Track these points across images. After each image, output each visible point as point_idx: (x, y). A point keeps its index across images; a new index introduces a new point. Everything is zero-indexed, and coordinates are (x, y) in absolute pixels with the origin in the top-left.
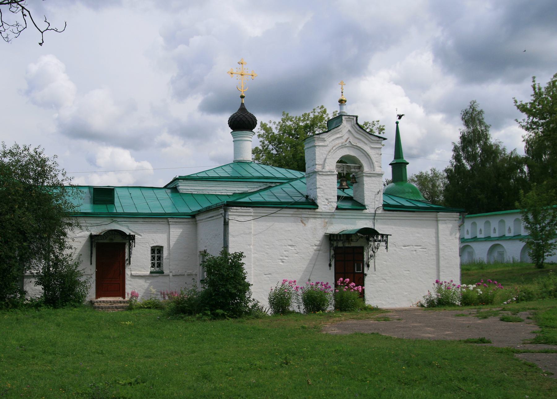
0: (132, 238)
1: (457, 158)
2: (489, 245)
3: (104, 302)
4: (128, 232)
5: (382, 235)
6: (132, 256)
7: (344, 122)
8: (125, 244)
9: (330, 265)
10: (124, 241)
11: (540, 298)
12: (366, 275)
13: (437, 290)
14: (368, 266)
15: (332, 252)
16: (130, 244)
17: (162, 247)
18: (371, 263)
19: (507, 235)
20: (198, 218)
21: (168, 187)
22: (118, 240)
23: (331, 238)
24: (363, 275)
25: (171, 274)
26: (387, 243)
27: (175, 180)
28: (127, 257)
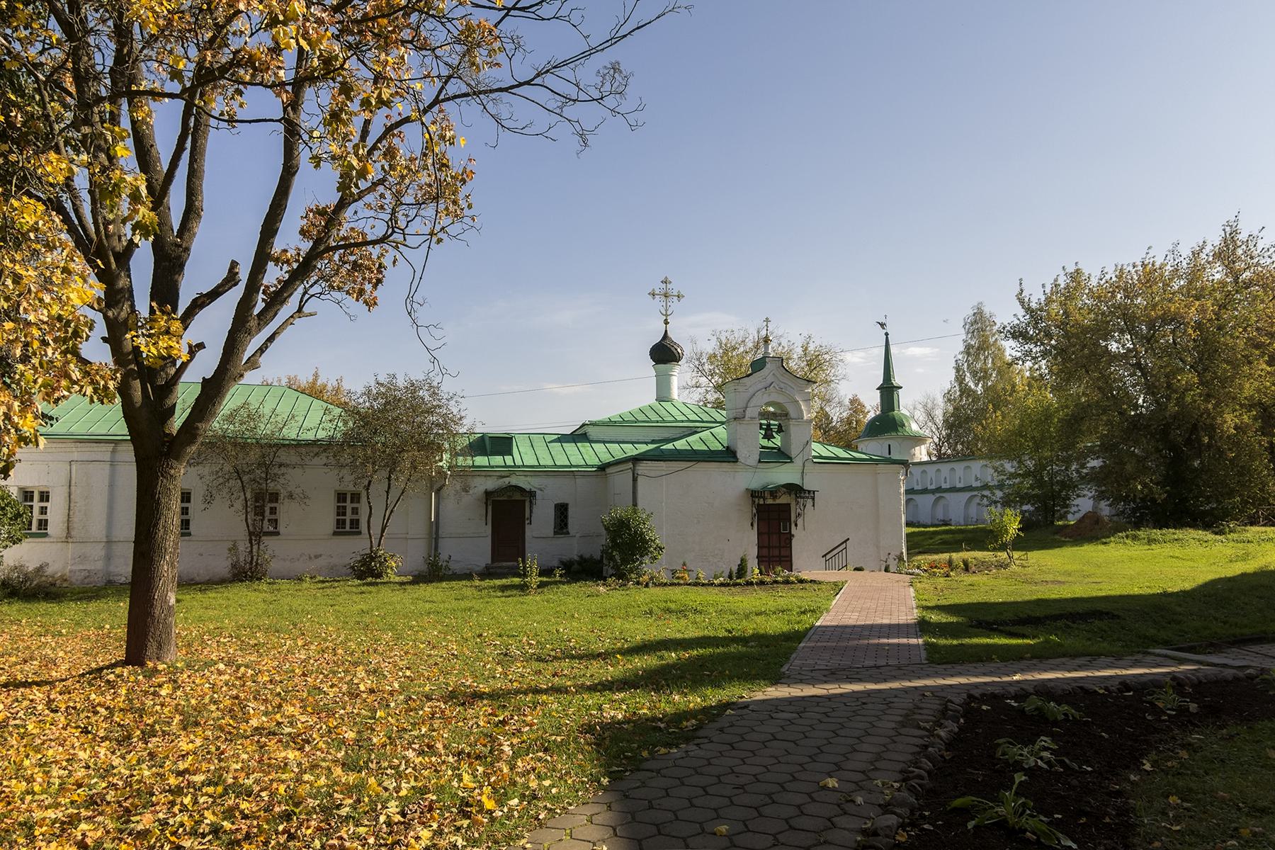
0: (532, 494)
1: (960, 379)
2: (968, 495)
3: (500, 567)
4: (527, 487)
5: (809, 492)
6: (533, 515)
7: (768, 366)
8: (525, 500)
9: (752, 525)
10: (523, 498)
11: (314, 457)
12: (793, 536)
13: (220, 432)
14: (796, 525)
15: (755, 511)
16: (531, 502)
17: (567, 504)
18: (800, 522)
19: (944, 486)
20: (609, 470)
21: (442, 97)
22: (517, 497)
23: (754, 494)
24: (791, 536)
25: (578, 535)
26: (813, 499)
27: (583, 425)
28: (527, 515)
